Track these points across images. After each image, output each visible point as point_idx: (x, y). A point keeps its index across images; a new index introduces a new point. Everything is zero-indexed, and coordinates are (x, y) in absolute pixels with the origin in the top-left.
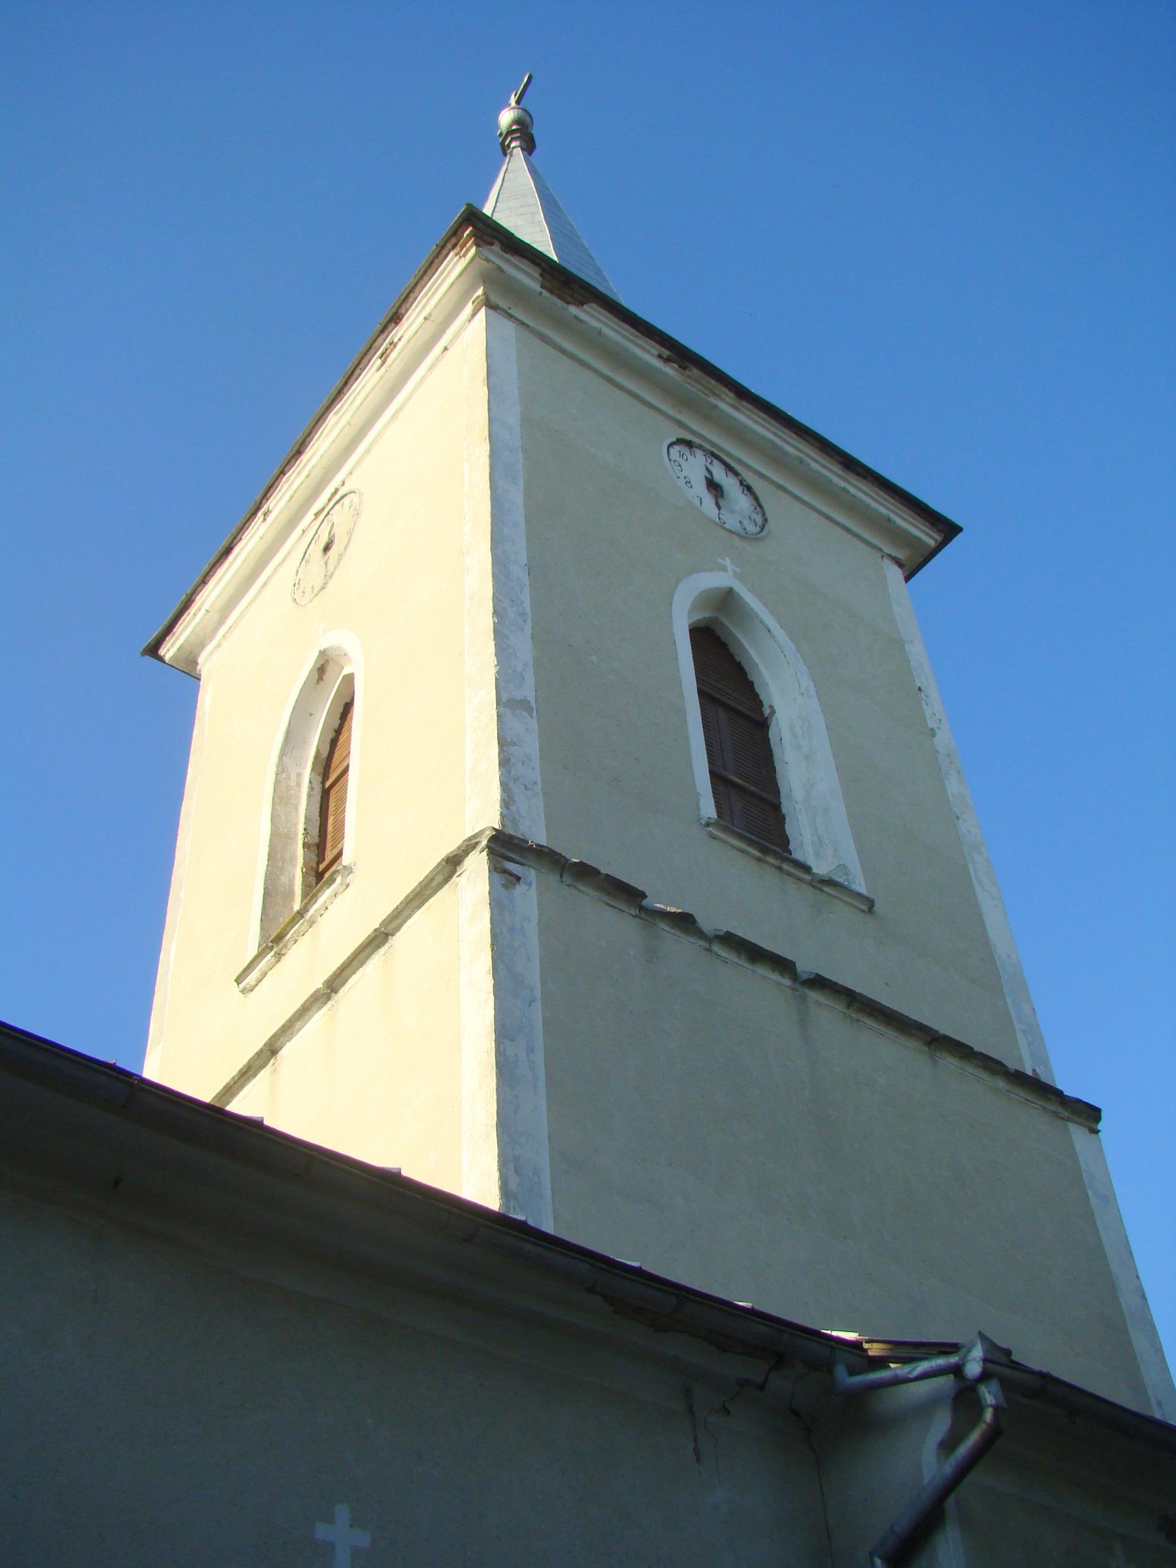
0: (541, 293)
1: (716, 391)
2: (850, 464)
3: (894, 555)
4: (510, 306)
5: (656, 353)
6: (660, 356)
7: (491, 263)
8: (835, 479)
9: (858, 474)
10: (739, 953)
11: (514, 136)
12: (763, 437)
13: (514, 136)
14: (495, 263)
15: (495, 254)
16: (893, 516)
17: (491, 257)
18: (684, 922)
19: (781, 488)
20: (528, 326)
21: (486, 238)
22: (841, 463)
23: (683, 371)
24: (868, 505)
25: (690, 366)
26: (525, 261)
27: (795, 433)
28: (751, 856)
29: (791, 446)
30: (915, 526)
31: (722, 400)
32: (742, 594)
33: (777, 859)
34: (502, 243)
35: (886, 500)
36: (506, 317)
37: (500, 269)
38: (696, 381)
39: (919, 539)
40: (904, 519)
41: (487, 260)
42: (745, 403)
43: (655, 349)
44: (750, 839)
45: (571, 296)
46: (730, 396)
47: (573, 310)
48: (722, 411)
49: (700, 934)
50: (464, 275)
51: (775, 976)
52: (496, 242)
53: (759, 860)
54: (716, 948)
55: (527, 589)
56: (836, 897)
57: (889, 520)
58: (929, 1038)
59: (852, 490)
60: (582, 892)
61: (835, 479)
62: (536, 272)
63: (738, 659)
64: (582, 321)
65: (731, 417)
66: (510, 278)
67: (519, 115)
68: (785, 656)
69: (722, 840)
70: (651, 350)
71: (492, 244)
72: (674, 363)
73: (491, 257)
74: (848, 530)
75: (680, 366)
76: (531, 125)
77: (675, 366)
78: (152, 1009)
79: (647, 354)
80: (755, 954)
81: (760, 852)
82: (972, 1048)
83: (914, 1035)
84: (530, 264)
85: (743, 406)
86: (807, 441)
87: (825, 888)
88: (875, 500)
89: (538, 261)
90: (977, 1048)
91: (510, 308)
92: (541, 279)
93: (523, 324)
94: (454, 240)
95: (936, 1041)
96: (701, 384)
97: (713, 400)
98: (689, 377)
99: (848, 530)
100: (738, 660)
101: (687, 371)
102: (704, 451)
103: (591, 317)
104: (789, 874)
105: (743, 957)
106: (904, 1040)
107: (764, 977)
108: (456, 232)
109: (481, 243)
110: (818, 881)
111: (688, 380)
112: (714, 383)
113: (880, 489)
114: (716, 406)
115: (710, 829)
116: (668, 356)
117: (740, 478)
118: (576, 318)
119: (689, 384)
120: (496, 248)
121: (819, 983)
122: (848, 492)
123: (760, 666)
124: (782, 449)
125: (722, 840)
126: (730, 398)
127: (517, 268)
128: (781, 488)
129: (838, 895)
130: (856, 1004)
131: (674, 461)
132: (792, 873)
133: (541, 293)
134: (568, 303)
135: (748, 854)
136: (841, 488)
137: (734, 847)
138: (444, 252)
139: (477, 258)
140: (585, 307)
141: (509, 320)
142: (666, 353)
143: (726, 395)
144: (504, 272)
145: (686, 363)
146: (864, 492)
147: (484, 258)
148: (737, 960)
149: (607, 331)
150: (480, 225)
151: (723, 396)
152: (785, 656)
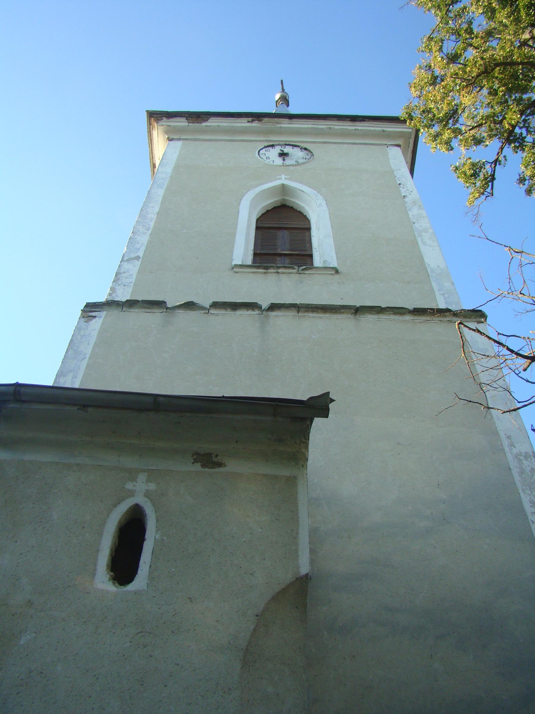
0: (188, 125)
1: (279, 122)
2: (354, 119)
3: (394, 144)
4: (180, 136)
5: (246, 121)
6: (249, 122)
7: (164, 126)
8: (350, 128)
9: (360, 121)
10: (226, 309)
11: (279, 102)
12: (307, 128)
13: (279, 102)
14: (166, 125)
15: (165, 122)
16: (385, 129)
17: (163, 124)
18: (190, 306)
19: (325, 143)
20: (188, 139)
21: (159, 119)
22: (350, 121)
23: (261, 122)
24: (370, 130)
25: (263, 119)
26: (178, 118)
27: (323, 120)
28: (260, 273)
29: (322, 125)
30: (399, 128)
31: (283, 124)
32: (290, 185)
33: (275, 269)
34: (166, 117)
35: (380, 125)
36: (178, 141)
37: (168, 125)
38: (268, 122)
39: (403, 132)
40: (389, 127)
41: (162, 125)
42: (294, 120)
43: (245, 120)
44: (256, 266)
45: (203, 120)
46: (287, 121)
47: (204, 124)
48: (283, 127)
49: (202, 308)
50: (159, 136)
51: (250, 312)
52: (163, 118)
53: (265, 273)
54: (212, 311)
55: (155, 220)
56: (315, 274)
57: (383, 131)
58: (353, 311)
59: (360, 128)
60: (131, 312)
61: (350, 128)
62: (184, 119)
63: (298, 210)
64: (209, 126)
65: (291, 128)
66: (175, 127)
67: (281, 95)
68: (311, 197)
69: (242, 272)
70: (244, 121)
71: (163, 119)
72: (256, 121)
73: (163, 124)
74: (365, 144)
75: (259, 121)
76: (287, 95)
77: (257, 121)
78: (322, 394)
79: (243, 123)
80: (235, 306)
81: (264, 269)
82: (381, 307)
83: (343, 312)
84: (180, 118)
85: (293, 121)
86: (328, 120)
87: (306, 272)
88: (377, 127)
89: (183, 115)
90: (383, 306)
91: (180, 137)
92: (187, 121)
93: (186, 139)
94: (151, 127)
95: (357, 311)
96: (271, 122)
97: (278, 126)
98: (265, 123)
99: (365, 144)
100: (299, 210)
101: (263, 121)
102: (281, 145)
103: (213, 122)
104: (283, 273)
105: (229, 310)
106: (339, 316)
107: (241, 315)
108: (150, 124)
109: (158, 121)
110: (301, 270)
111: (265, 124)
112: (276, 119)
113: (374, 122)
114: (281, 127)
115: (234, 270)
116: (252, 120)
117: (300, 147)
118: (206, 126)
119: (265, 125)
120: (165, 119)
121: (273, 307)
122: (358, 130)
123: (305, 207)
124: (318, 128)
125: (242, 272)
126: (286, 121)
127: (174, 122)
128: (325, 143)
129: (315, 272)
130: (302, 309)
131: (262, 154)
132: (259, 271)
133: (188, 125)
134: (201, 123)
135: (258, 273)
136: (354, 129)
137: (250, 273)
138: (152, 133)
139: (159, 127)
140: (209, 121)
141: (180, 141)
142: (250, 119)
143: (284, 121)
144: (170, 126)
145: (261, 118)
146: (367, 126)
147: (160, 125)
148: (226, 313)
149: (220, 124)
150: (155, 116)
151: (283, 122)
152: (311, 197)
